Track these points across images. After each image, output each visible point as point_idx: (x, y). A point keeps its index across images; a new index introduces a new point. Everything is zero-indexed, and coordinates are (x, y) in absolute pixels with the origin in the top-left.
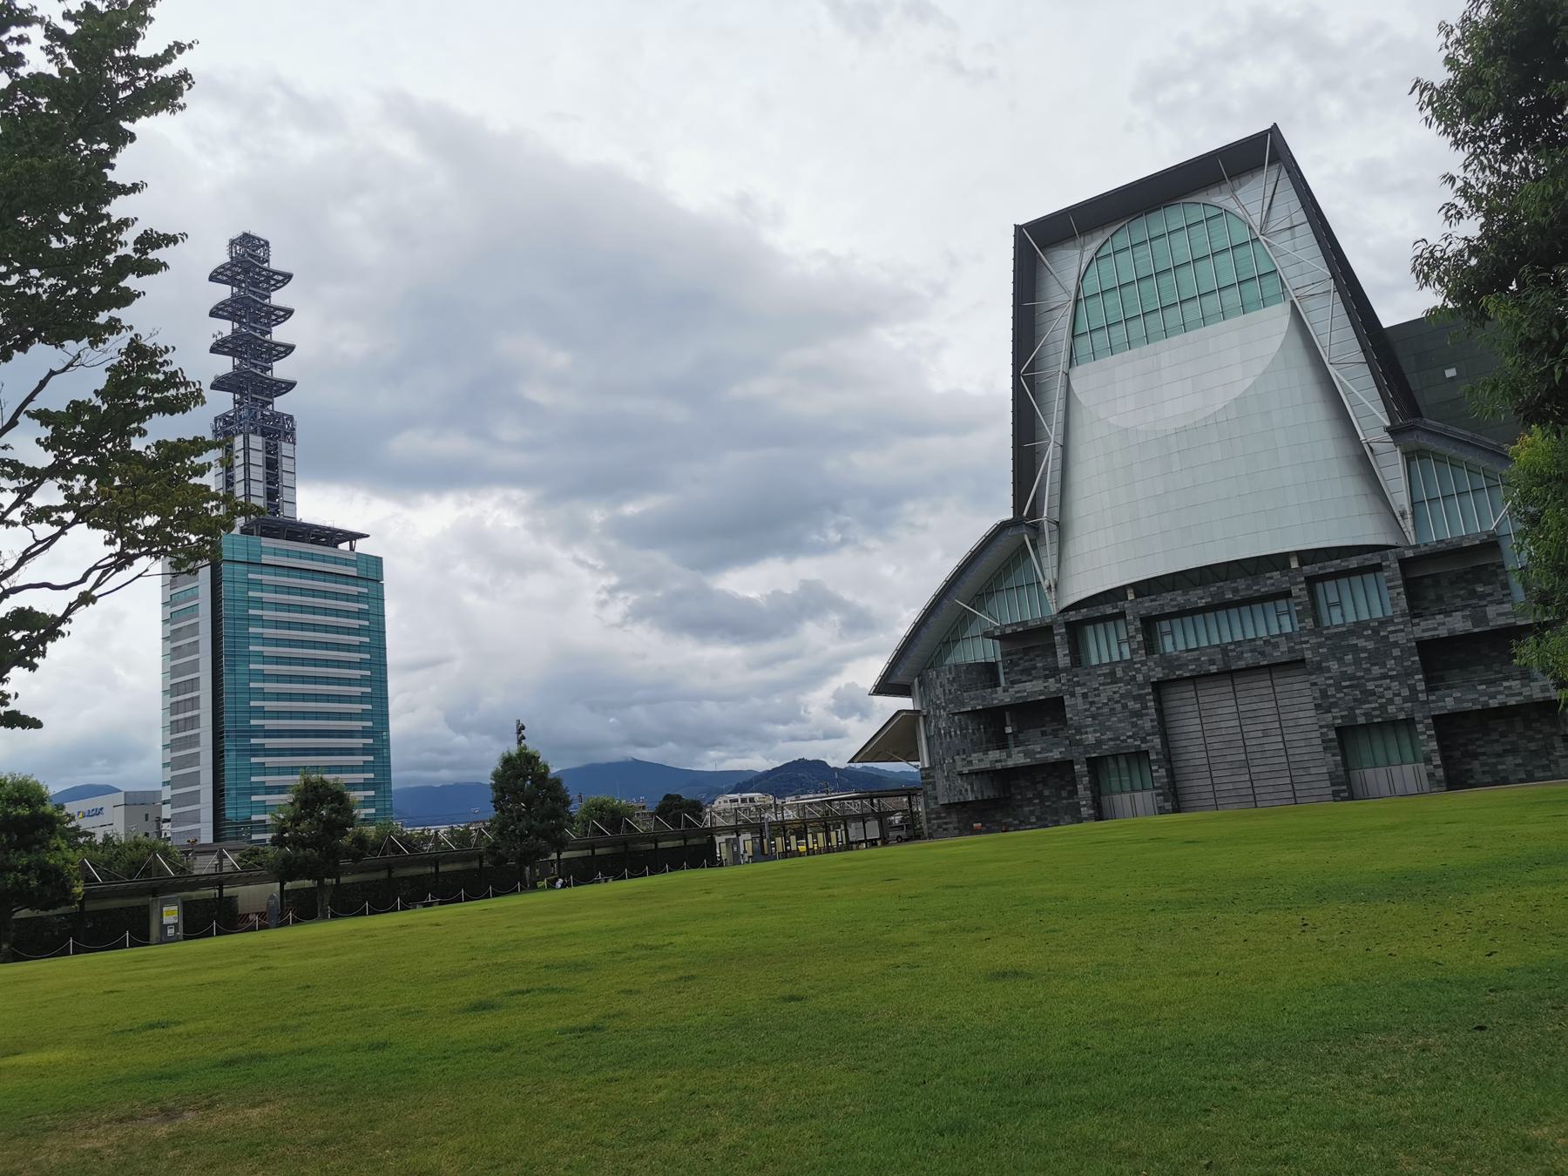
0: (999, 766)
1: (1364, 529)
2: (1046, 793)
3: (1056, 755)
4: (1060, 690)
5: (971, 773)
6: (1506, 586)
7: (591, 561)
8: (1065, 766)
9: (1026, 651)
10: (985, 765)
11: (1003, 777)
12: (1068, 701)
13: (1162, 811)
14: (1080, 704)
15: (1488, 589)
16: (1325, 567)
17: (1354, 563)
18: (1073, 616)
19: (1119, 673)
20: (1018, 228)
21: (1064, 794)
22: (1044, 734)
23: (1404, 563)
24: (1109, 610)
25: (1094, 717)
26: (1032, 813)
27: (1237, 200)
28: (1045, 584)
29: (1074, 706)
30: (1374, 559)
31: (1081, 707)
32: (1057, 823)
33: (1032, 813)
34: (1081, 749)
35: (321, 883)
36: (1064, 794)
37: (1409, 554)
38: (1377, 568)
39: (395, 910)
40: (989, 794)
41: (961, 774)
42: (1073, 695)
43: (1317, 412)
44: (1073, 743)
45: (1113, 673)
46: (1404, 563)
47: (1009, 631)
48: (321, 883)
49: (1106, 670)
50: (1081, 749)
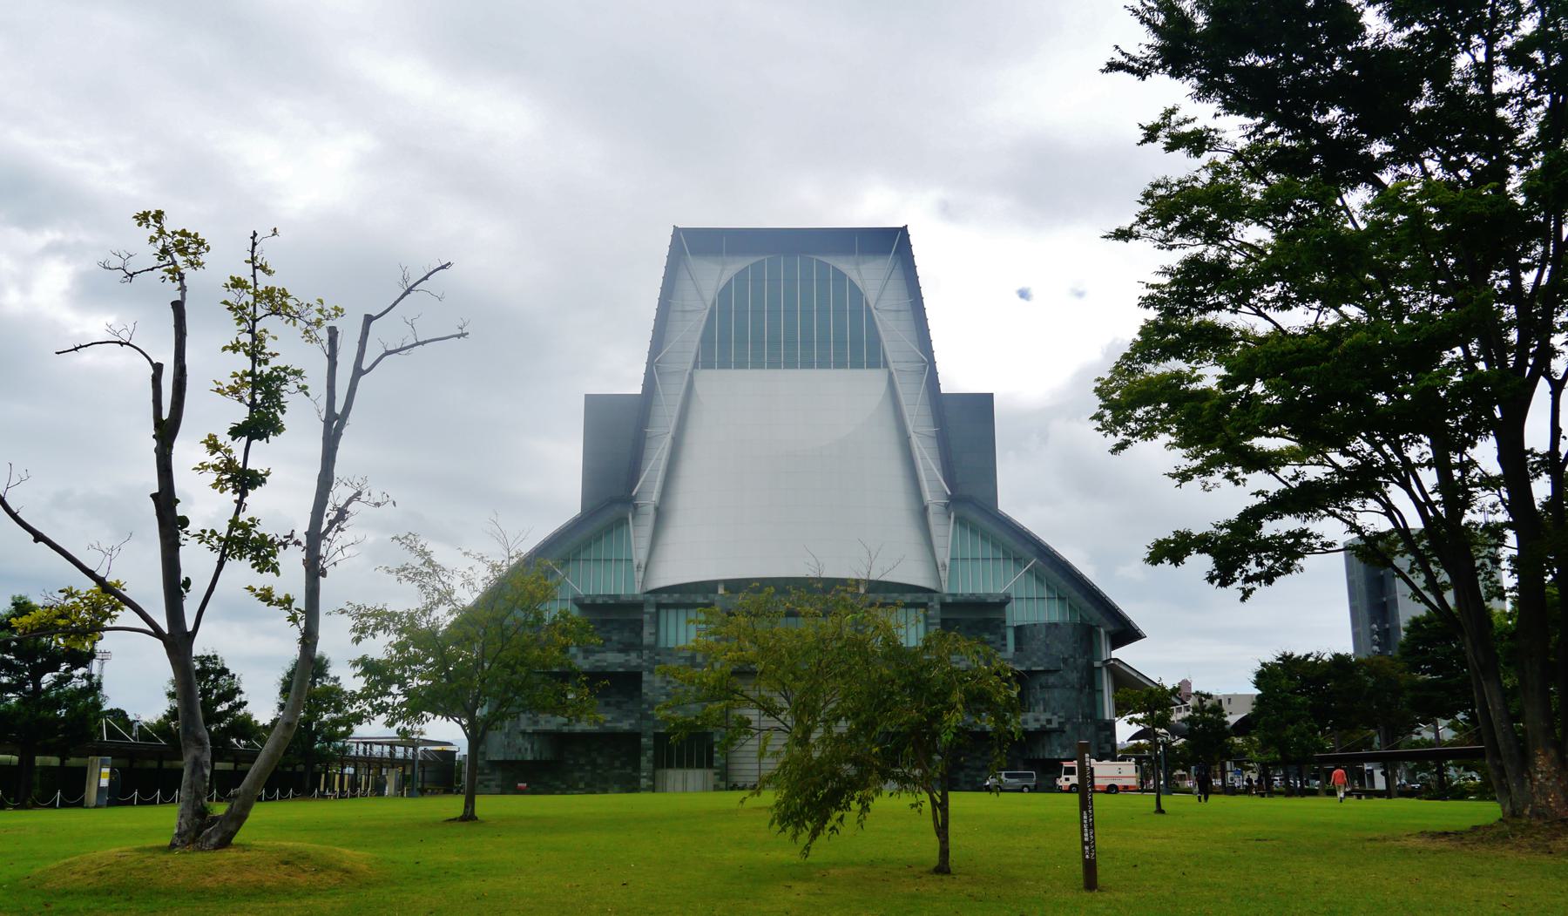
0: (565, 729)
1: (913, 572)
2: (600, 761)
3: (625, 725)
4: (639, 666)
5: (535, 733)
6: (1004, 638)
7: (928, 497)
8: (633, 738)
9: (604, 623)
10: (549, 727)
11: (560, 740)
12: (646, 676)
13: (716, 788)
14: (657, 680)
15: (993, 638)
16: (887, 593)
17: (908, 598)
18: (665, 598)
19: (699, 659)
20: (677, 230)
21: (617, 764)
22: (607, 704)
23: (944, 605)
24: (700, 600)
25: (668, 695)
26: (581, 778)
27: (859, 273)
28: (636, 562)
29: (652, 683)
30: (923, 598)
31: (657, 684)
32: (605, 791)
33: (581, 778)
34: (651, 724)
35: (27, 761)
36: (617, 764)
37: (949, 600)
38: (924, 605)
39: (53, 806)
40: (547, 755)
41: (524, 733)
42: (651, 672)
43: (893, 469)
44: (645, 716)
45: (693, 658)
46: (944, 605)
47: (599, 601)
48: (27, 761)
49: (688, 654)
50: (651, 724)
